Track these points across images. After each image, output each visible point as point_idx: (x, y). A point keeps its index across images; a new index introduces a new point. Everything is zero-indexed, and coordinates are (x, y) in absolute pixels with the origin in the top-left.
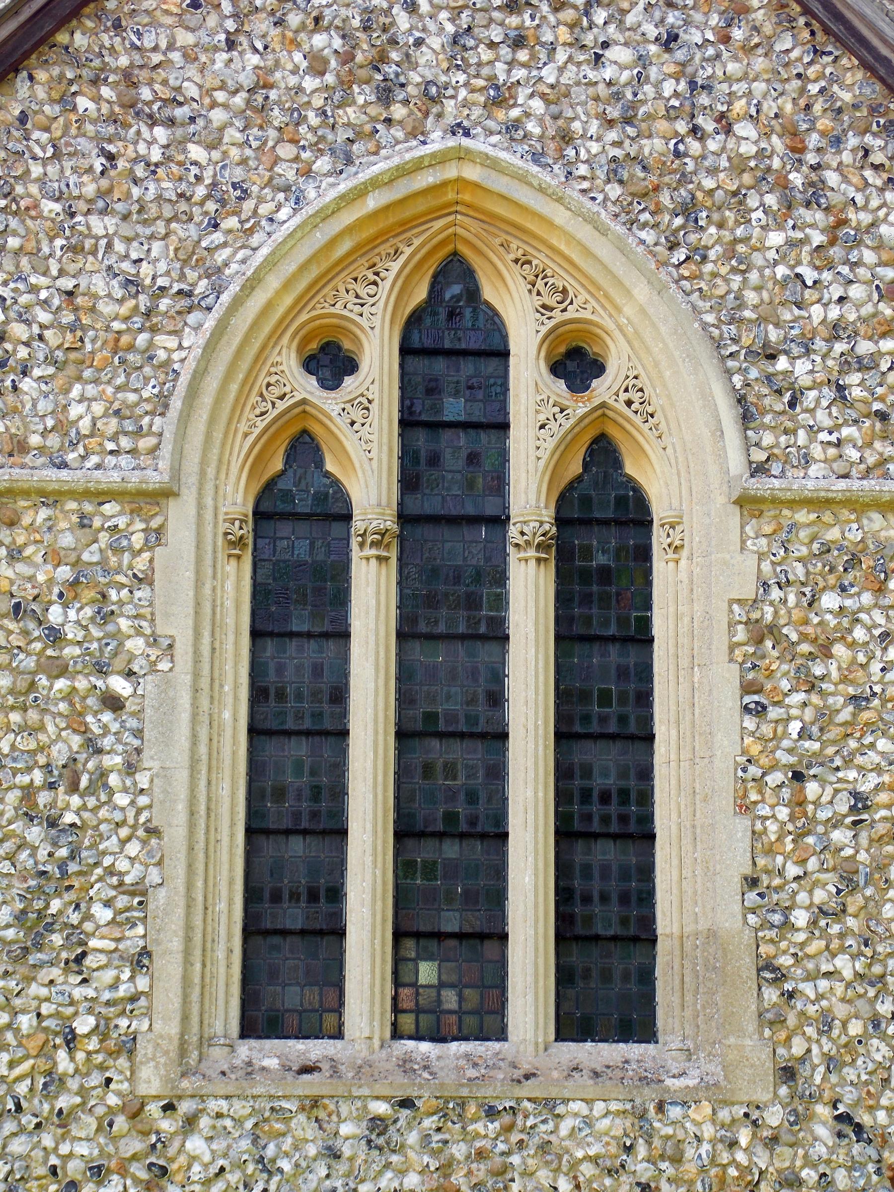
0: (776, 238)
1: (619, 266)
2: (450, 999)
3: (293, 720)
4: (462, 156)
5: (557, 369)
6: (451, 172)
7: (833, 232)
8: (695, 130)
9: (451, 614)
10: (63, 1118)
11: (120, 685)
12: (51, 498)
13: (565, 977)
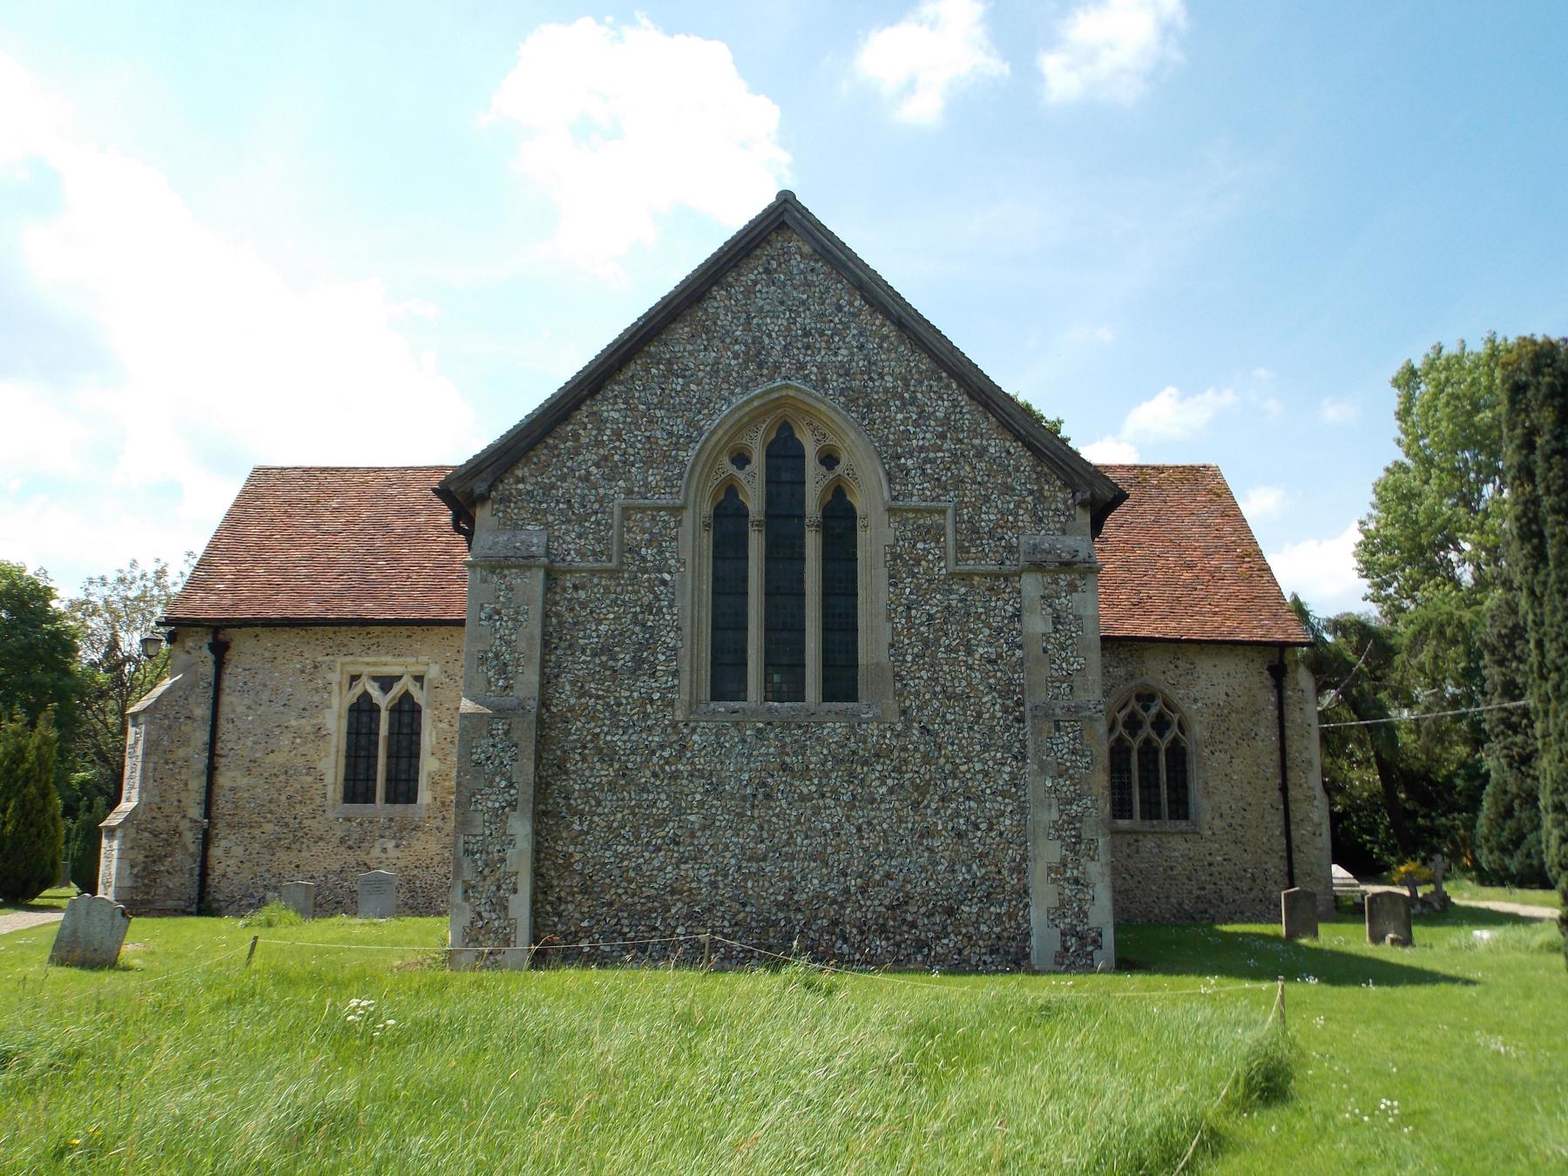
0: (900, 416)
1: (844, 425)
2: (785, 687)
3: (728, 587)
4: (787, 387)
5: (822, 462)
6: (784, 393)
7: (920, 414)
8: (871, 379)
9: (784, 552)
10: (650, 728)
11: (667, 577)
12: (642, 510)
13: (825, 680)
